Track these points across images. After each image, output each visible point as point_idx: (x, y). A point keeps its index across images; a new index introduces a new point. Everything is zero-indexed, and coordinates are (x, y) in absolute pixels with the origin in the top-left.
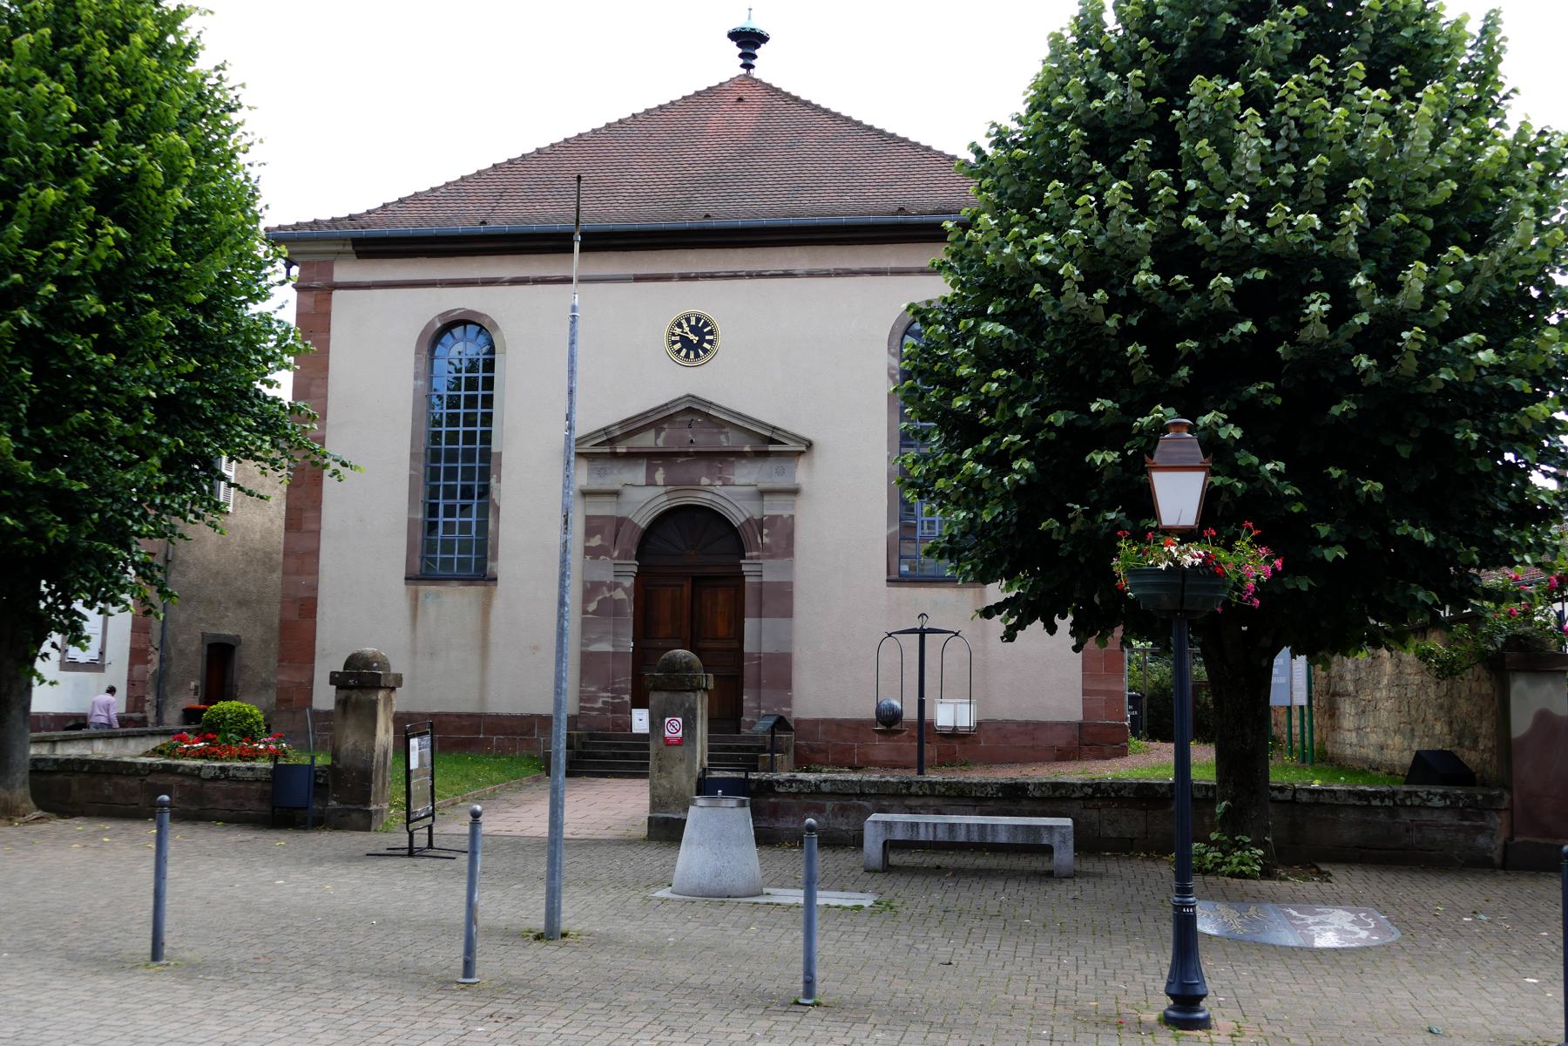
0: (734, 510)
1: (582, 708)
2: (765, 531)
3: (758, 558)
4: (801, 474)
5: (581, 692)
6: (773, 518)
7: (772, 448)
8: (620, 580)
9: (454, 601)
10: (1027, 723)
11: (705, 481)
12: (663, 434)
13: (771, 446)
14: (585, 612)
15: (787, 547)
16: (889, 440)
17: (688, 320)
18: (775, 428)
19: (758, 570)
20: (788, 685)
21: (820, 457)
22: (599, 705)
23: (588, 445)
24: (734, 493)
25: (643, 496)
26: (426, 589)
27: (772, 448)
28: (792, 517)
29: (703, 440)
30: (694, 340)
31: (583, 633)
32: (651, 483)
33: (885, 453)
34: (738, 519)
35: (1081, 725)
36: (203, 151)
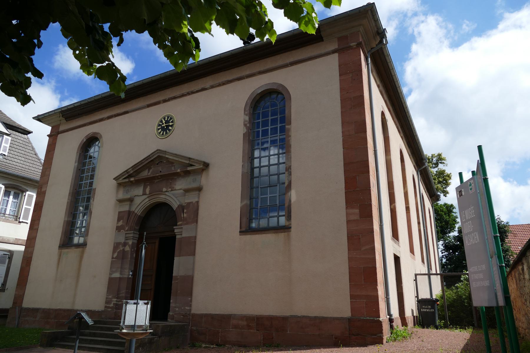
0: (171, 200)
1: (106, 307)
2: (185, 211)
3: (181, 225)
4: (204, 180)
5: (107, 298)
6: (189, 204)
7: (189, 169)
8: (127, 241)
9: (72, 254)
10: (316, 318)
11: (164, 190)
12: (151, 171)
13: (193, 169)
14: (113, 258)
15: (195, 218)
16: (243, 157)
17: (164, 119)
18: (190, 158)
19: (183, 232)
20: (190, 294)
21: (212, 171)
22: (112, 305)
23: (121, 179)
24: (174, 196)
25: (141, 199)
26: (65, 251)
27: (189, 169)
28: (198, 202)
29: (163, 170)
30: (166, 127)
31: (111, 268)
32: (144, 194)
33: (241, 164)
34: (175, 205)
35: (349, 320)
36: (437, 228)
